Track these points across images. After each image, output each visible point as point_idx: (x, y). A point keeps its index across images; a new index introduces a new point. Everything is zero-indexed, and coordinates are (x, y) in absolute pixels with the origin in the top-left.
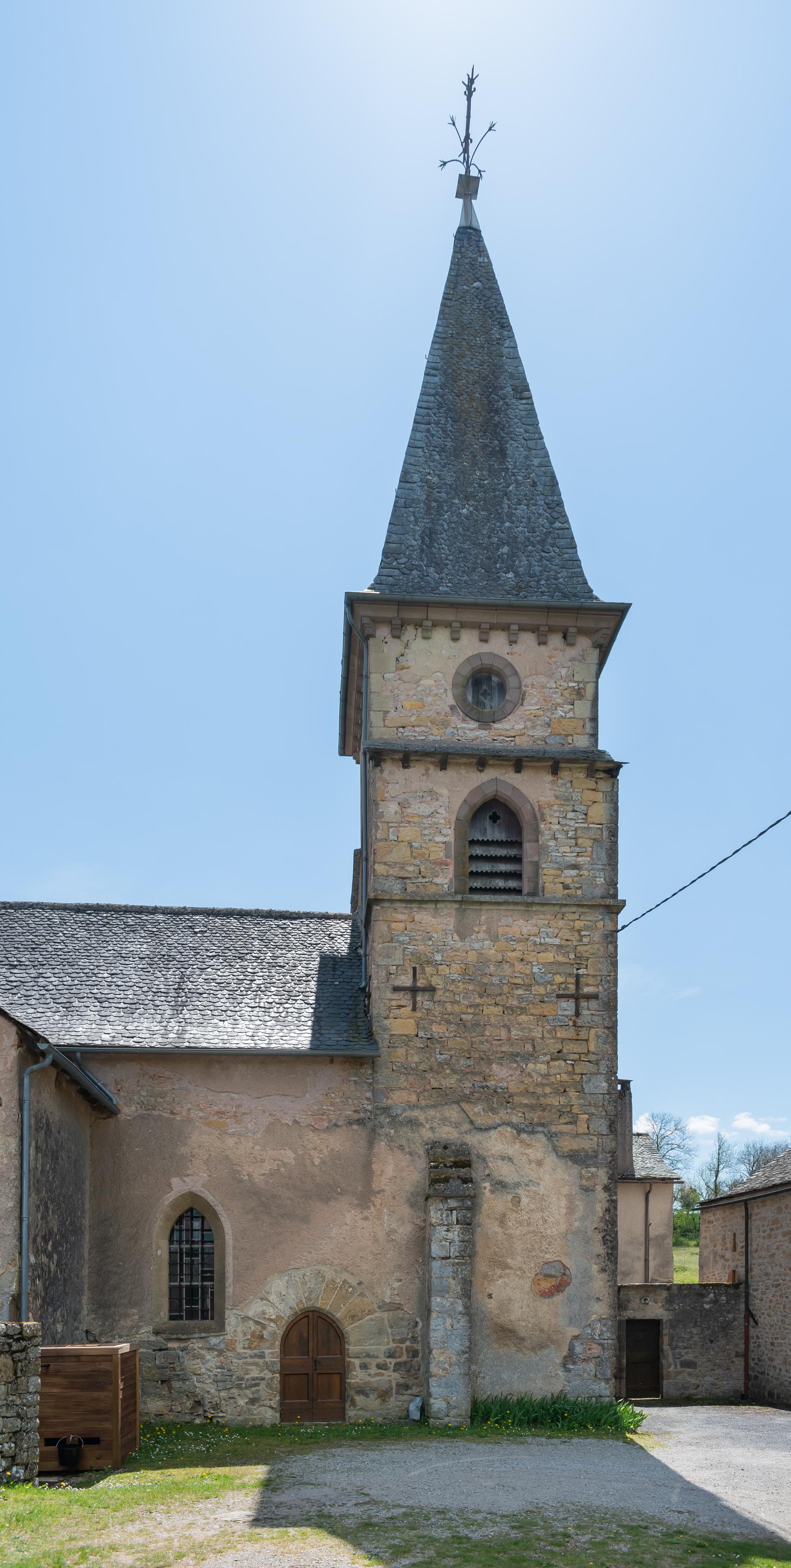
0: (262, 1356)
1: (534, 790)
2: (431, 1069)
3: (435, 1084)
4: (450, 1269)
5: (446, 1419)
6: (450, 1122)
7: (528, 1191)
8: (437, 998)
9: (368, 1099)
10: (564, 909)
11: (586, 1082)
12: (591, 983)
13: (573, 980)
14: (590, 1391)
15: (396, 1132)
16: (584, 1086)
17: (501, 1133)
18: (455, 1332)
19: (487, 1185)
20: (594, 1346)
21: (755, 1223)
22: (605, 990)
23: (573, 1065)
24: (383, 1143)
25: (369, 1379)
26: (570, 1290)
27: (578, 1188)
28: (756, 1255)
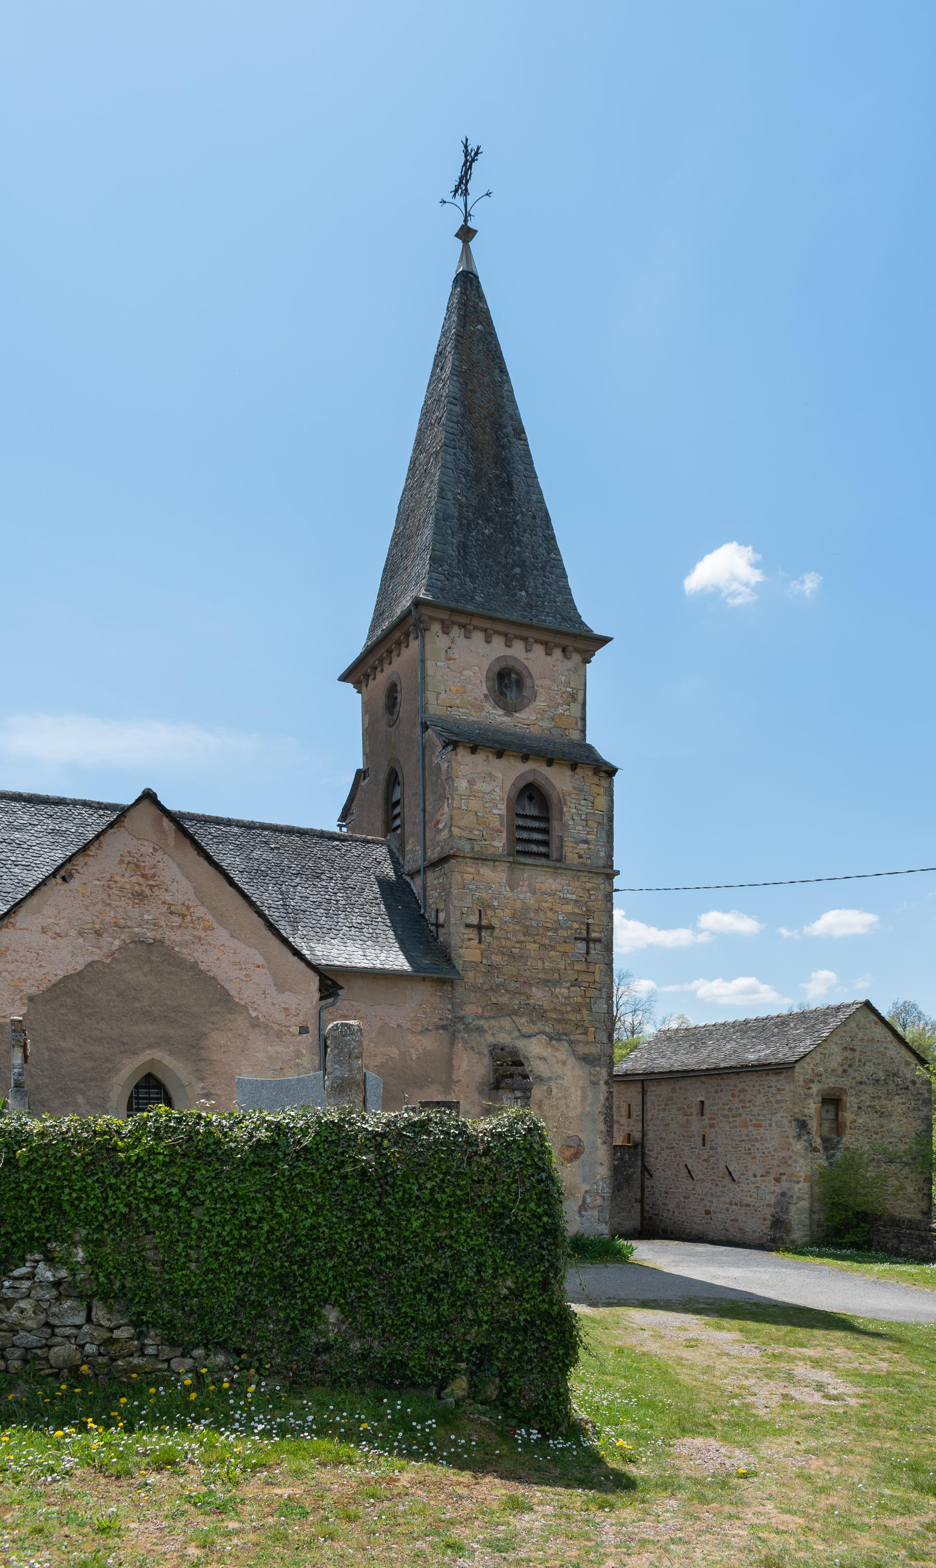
1: (559, 780)
2: (492, 989)
3: (494, 1001)
8: (495, 934)
9: (449, 1010)
10: (579, 874)
13: (585, 927)
17: (539, 1040)
20: (598, 1198)
21: (650, 1098)
26: (583, 1157)
28: (651, 1123)
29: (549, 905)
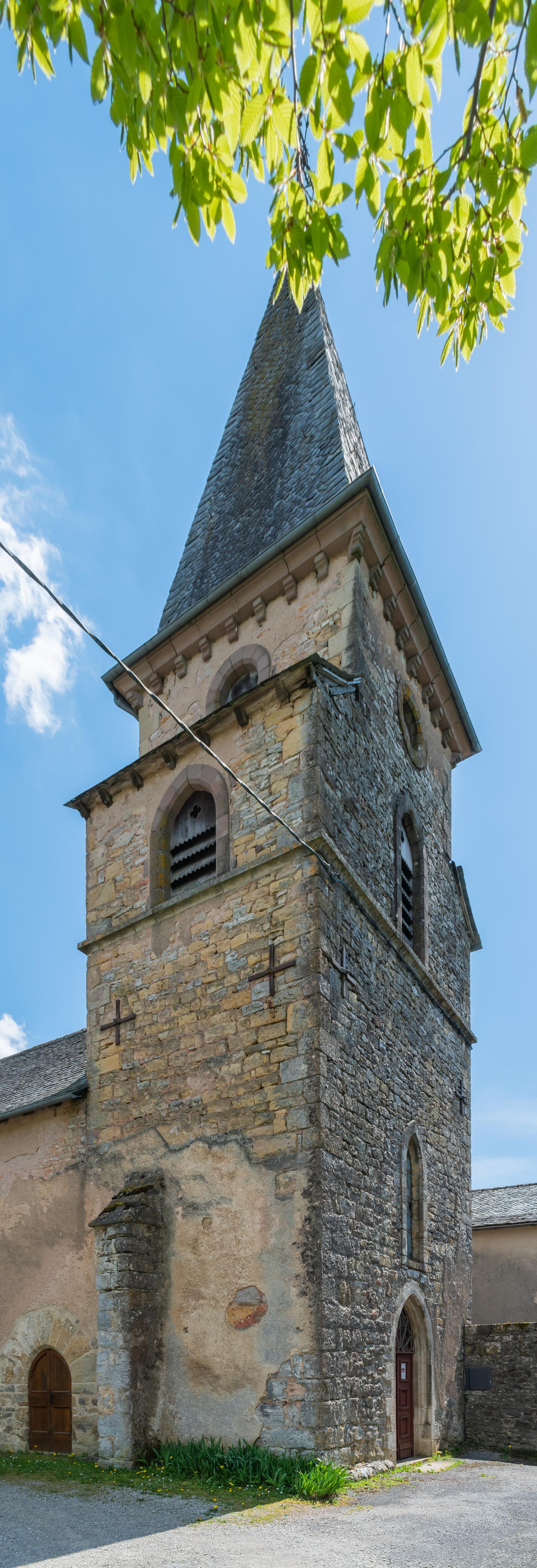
0: (12, 1390)
2: (133, 1100)
3: (136, 1113)
4: (111, 1301)
5: (111, 1460)
6: (147, 1150)
7: (220, 1210)
8: (137, 1026)
9: (82, 1143)
11: (283, 1070)
12: (288, 950)
14: (292, 1441)
15: (102, 1169)
16: (281, 1075)
17: (193, 1150)
18: (117, 1368)
19: (179, 1209)
20: (297, 1386)
22: (304, 952)
23: (269, 1054)
24: (92, 1183)
25: (86, 1414)
26: (265, 1320)
27: (273, 1198)
29: (211, 949)
